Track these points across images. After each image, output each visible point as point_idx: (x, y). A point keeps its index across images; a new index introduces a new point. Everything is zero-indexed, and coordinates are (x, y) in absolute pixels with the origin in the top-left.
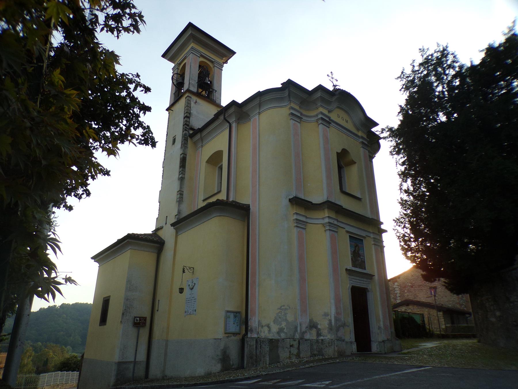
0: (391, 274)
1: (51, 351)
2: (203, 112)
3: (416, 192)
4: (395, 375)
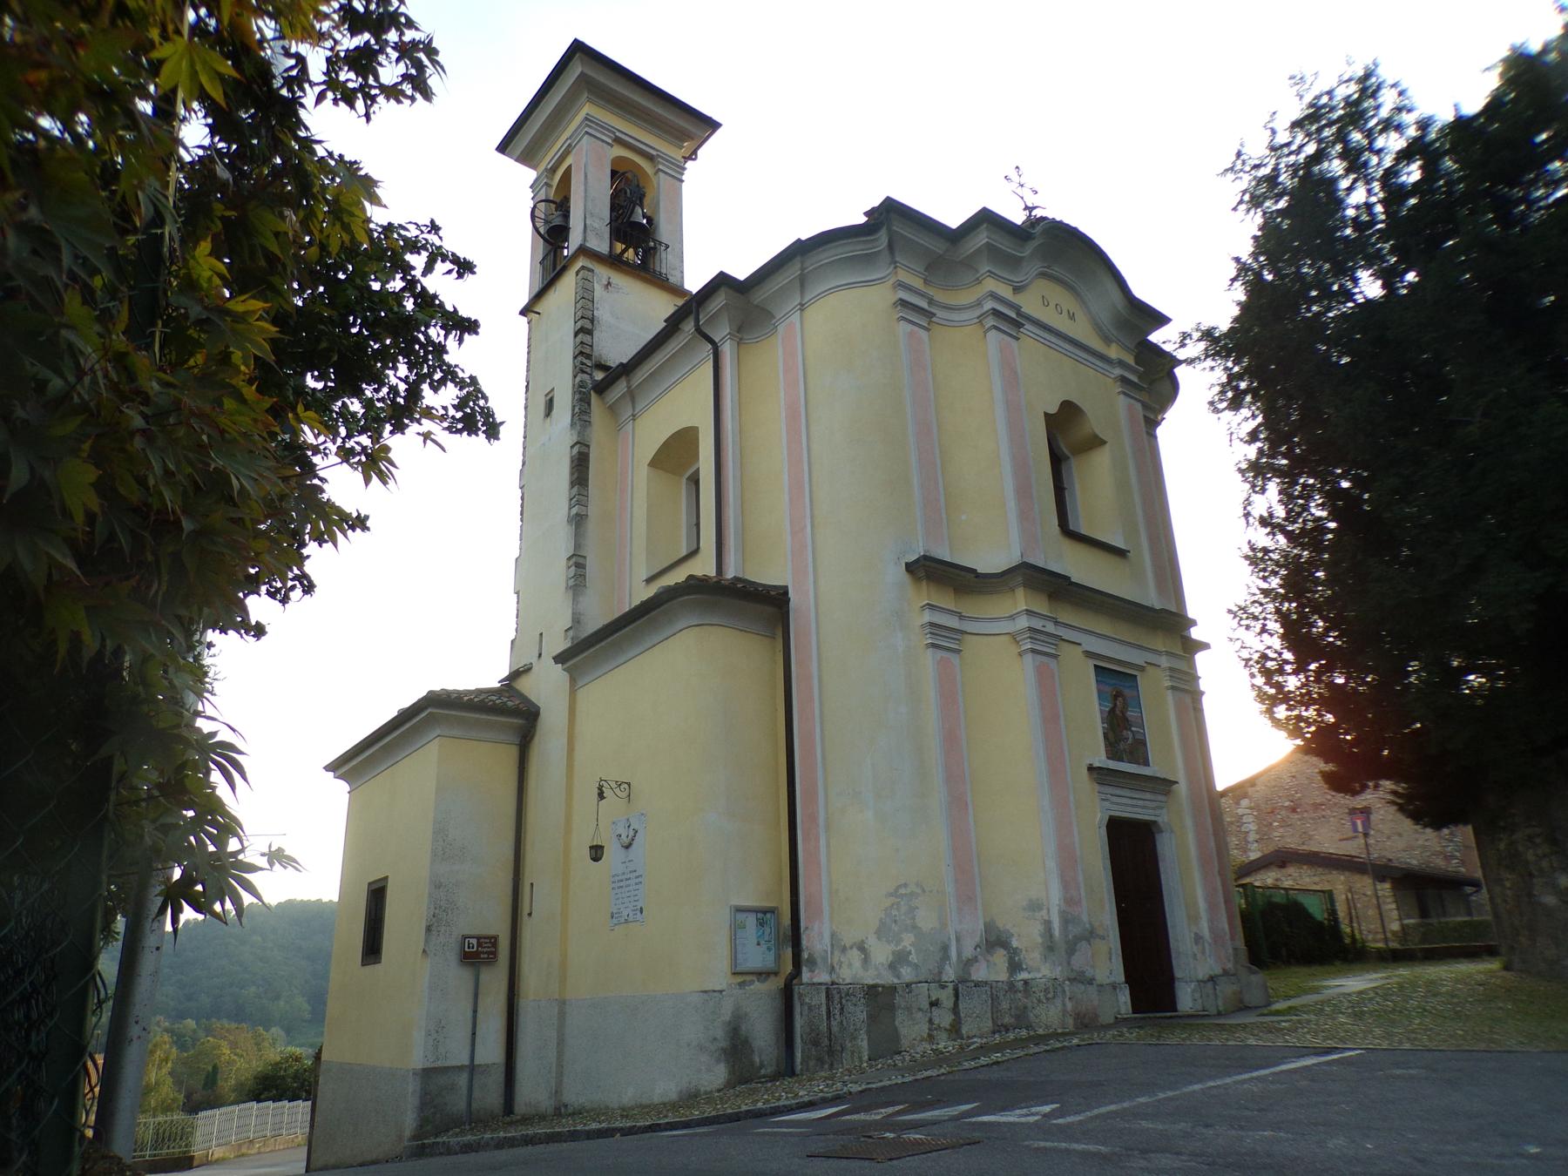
0: (1225, 776)
1: (224, 1043)
2: (631, 314)
3: (1294, 522)
4: (1251, 1079)
